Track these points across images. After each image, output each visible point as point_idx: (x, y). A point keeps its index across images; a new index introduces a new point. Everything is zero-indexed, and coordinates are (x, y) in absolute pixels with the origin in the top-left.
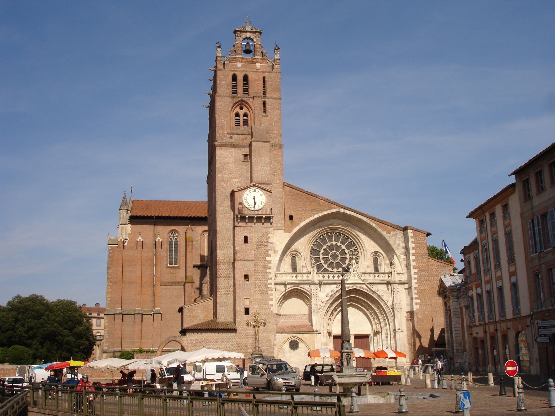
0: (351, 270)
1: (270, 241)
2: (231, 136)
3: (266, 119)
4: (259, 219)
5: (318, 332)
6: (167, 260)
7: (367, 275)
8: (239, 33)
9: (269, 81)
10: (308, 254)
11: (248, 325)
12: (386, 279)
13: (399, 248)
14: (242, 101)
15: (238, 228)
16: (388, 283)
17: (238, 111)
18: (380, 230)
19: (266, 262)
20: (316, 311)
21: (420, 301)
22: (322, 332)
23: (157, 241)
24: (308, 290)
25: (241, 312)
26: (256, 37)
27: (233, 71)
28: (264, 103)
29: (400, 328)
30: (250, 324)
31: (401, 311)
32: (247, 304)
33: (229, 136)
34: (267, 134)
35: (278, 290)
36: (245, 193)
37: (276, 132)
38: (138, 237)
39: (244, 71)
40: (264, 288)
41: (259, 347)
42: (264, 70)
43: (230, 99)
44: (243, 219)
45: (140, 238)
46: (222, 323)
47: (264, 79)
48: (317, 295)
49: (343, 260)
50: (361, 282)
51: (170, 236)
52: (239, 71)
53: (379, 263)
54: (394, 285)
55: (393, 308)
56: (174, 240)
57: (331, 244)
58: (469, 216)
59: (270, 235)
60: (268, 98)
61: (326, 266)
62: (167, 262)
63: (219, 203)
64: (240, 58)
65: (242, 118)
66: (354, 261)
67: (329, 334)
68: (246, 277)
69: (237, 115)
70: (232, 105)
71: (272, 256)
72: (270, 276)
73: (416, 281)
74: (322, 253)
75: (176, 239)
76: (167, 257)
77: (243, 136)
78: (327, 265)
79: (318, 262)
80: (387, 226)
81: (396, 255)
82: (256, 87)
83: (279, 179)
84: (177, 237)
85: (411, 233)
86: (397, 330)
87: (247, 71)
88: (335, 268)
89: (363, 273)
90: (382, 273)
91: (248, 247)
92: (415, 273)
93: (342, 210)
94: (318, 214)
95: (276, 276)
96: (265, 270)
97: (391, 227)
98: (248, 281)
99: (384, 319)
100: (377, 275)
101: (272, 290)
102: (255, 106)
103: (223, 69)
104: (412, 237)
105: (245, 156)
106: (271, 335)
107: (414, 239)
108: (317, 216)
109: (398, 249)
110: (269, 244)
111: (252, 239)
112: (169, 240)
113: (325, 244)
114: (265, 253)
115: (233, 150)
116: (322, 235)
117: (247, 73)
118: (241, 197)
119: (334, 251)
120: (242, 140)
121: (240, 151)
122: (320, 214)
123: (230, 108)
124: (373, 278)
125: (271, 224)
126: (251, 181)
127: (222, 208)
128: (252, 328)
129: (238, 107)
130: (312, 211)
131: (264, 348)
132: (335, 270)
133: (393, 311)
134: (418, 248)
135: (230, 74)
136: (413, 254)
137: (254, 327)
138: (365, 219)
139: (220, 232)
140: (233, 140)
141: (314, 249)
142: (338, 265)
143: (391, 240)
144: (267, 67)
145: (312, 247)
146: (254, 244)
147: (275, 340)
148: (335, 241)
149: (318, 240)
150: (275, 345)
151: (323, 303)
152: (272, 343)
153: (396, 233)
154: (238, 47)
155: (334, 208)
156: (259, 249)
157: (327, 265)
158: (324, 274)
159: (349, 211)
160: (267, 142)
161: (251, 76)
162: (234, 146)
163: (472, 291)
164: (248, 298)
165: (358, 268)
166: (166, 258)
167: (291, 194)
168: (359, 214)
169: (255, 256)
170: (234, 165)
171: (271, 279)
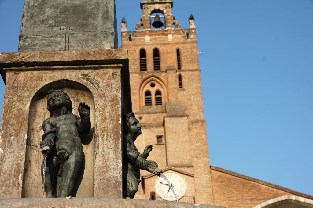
3: (182, 93)
14: (153, 76)
28: (180, 77)
39: (154, 44)
42: (178, 41)
47: (178, 51)
60: (183, 71)
65: (153, 97)
69: (148, 93)
70: (140, 82)
83: (204, 163)
87: (157, 44)
93: (294, 197)
94: (260, 203)
117: (158, 47)
118: (153, 185)
120: (154, 120)
121: (152, 132)
123: (138, 85)
135: (137, 49)
155: (282, 195)
160: (183, 116)
161: (161, 49)
167: (220, 179)
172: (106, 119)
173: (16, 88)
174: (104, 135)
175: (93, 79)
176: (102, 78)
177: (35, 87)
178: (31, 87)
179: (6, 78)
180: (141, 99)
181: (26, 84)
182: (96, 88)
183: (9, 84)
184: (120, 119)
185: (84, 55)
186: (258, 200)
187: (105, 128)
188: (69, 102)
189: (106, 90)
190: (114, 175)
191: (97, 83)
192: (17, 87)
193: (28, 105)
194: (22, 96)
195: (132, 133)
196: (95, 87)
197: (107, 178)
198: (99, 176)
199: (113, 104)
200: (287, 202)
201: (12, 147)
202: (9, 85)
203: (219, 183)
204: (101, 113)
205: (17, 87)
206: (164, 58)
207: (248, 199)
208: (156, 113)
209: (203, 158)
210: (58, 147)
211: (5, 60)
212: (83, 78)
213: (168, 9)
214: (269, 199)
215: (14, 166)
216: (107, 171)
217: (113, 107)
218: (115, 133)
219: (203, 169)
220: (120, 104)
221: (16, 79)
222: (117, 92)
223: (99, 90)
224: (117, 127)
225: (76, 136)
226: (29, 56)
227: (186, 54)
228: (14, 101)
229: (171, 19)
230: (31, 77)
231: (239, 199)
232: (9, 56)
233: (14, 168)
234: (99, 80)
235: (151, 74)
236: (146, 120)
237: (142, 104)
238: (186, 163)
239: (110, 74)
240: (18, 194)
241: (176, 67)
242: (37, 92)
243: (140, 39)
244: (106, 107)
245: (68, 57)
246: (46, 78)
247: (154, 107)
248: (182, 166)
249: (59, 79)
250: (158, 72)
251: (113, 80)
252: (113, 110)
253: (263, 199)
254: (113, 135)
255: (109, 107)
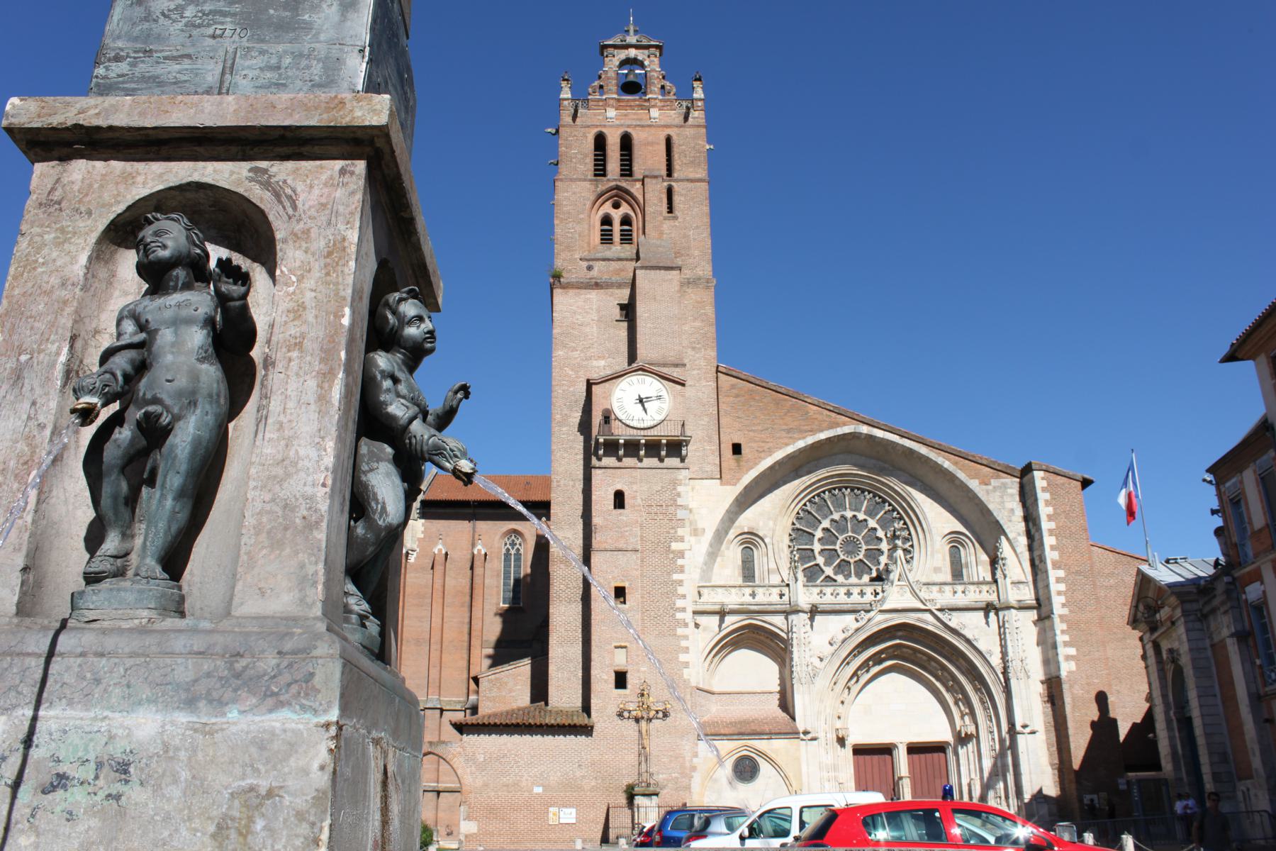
0: (894, 576)
1: (680, 501)
2: (591, 263)
3: (673, 224)
4: (653, 448)
5: (809, 736)
6: (498, 594)
7: (935, 588)
8: (610, 50)
9: (680, 145)
10: (782, 542)
11: (620, 715)
12: (987, 595)
13: (1014, 518)
14: (618, 188)
15: (598, 471)
16: (988, 608)
17: (608, 211)
18: (961, 475)
19: (671, 556)
20: (803, 681)
21: (1077, 650)
22: (821, 735)
23: (476, 552)
24: (785, 627)
25: (606, 681)
26: (649, 57)
27: (597, 126)
28: (670, 192)
29: (1028, 723)
30: (626, 714)
31: (1028, 677)
32: (620, 660)
33: (585, 264)
34: (676, 257)
35: (705, 629)
36: (619, 388)
37: (696, 253)
38: (436, 544)
39: (622, 125)
40: (666, 620)
41: (652, 775)
42: (669, 121)
43: (589, 186)
44: (611, 447)
45: (440, 546)
46: (560, 712)
47: (669, 141)
48: (807, 640)
49: (874, 554)
50: (923, 607)
51: (506, 544)
52: (611, 126)
53: (963, 561)
54: (1006, 612)
55: (1005, 672)
56: (513, 552)
57: (842, 516)
58: (1231, 357)
59: (680, 489)
60: (677, 181)
61: (829, 571)
62: (499, 599)
63: (558, 416)
64: (612, 99)
65: (617, 227)
66: (900, 553)
67: (841, 741)
68: (620, 593)
69: (607, 221)
70: (593, 198)
71: (686, 539)
72: (681, 590)
73: (1062, 599)
74: (819, 540)
75: (518, 550)
76: (498, 587)
77: (619, 263)
78: (832, 567)
79: (810, 561)
80: (979, 466)
81: (1008, 539)
82: (648, 158)
83: (705, 359)
84: (520, 545)
85: (1043, 479)
86: (1018, 728)
87: (629, 126)
88: (853, 575)
89: (924, 584)
90: (973, 584)
91: (625, 518)
92: (1058, 580)
93: (865, 429)
94: (804, 438)
95: (699, 592)
96: (669, 574)
97: (989, 469)
98: (624, 602)
99: (983, 702)
100: (960, 588)
101: (686, 625)
102: (647, 196)
103: (572, 123)
104: (1044, 490)
105: (623, 307)
106: (684, 742)
107: (1051, 494)
108: (801, 444)
109: (1010, 521)
110: (678, 511)
111: (634, 498)
112: (504, 551)
113: (825, 517)
114: (668, 533)
115: (593, 295)
116: (818, 495)
117: (629, 130)
118: (608, 396)
119: (850, 534)
120: (618, 272)
121: (610, 296)
122: (810, 440)
123: (589, 204)
124: (951, 594)
125: (683, 460)
126: (632, 357)
127: (564, 429)
128: (632, 722)
129: (607, 203)
130: (789, 431)
131: (664, 776)
132: (853, 580)
133: (1007, 680)
134: (1063, 516)
135: (589, 133)
136: (1051, 532)
137: (637, 720)
138: (923, 450)
139: (558, 486)
140: (594, 273)
141: (798, 529)
142: (861, 568)
143: (992, 500)
144: (675, 115)
145: (793, 524)
146: (641, 511)
147: (696, 755)
148: (851, 510)
149: (808, 508)
150: (694, 769)
151: (821, 660)
152: (688, 764)
153: (1002, 483)
154: (609, 78)
155: (844, 424)
156: (653, 522)
157: (832, 567)
158: (824, 588)
159: (882, 432)
160: (671, 268)
161: (638, 136)
162: (597, 285)
163: (1258, 583)
164: (625, 647)
165: (910, 571)
166: (495, 589)
167: (735, 391)
168: (909, 439)
169: (642, 540)
170: (595, 329)
171: (684, 596)
172: (305, 308)
173: (57, 206)
174: (290, 360)
175: (281, 183)
176: (308, 182)
177: (111, 205)
178: (98, 203)
179: (34, 175)
180: (592, 232)
181: (87, 195)
182: (287, 213)
183: (40, 191)
184: (347, 311)
185: (258, 112)
186: (801, 431)
187: (296, 338)
188: (197, 254)
189: (315, 218)
190: (307, 488)
191: (291, 196)
192: (59, 203)
193: (83, 259)
194: (70, 229)
195: (404, 348)
196: (284, 208)
197: (286, 500)
198: (261, 490)
199: (329, 264)
200: (854, 436)
201: (20, 385)
202: (39, 194)
203: (732, 399)
204: (291, 289)
205: (59, 203)
206: (640, 153)
207: (784, 430)
208: (620, 259)
209: (705, 349)
210: (144, 394)
211: (29, 120)
212: (251, 180)
213: (652, 58)
214: (822, 431)
215: (19, 445)
216: (288, 475)
217: (328, 274)
218: (327, 355)
219: (704, 371)
220: (350, 263)
221: (59, 178)
222: (349, 226)
223: (294, 220)
224: (332, 336)
225: (203, 362)
226: (97, 111)
227: (684, 147)
228: (46, 245)
229: (658, 77)
230: (104, 172)
231: (767, 429)
232: (43, 108)
233: (16, 452)
234: (300, 187)
235: (613, 184)
236: (600, 271)
237: (594, 240)
238: (673, 359)
239: (333, 169)
240: (20, 532)
241: (664, 172)
242: (115, 219)
243: (595, 115)
244: (309, 271)
245: (210, 114)
246: (146, 178)
247: (617, 249)
248: (659, 365)
249: (184, 181)
250: (627, 180)
251: (339, 189)
252: (328, 283)
253: (811, 431)
254: (317, 363)
255: (317, 273)
